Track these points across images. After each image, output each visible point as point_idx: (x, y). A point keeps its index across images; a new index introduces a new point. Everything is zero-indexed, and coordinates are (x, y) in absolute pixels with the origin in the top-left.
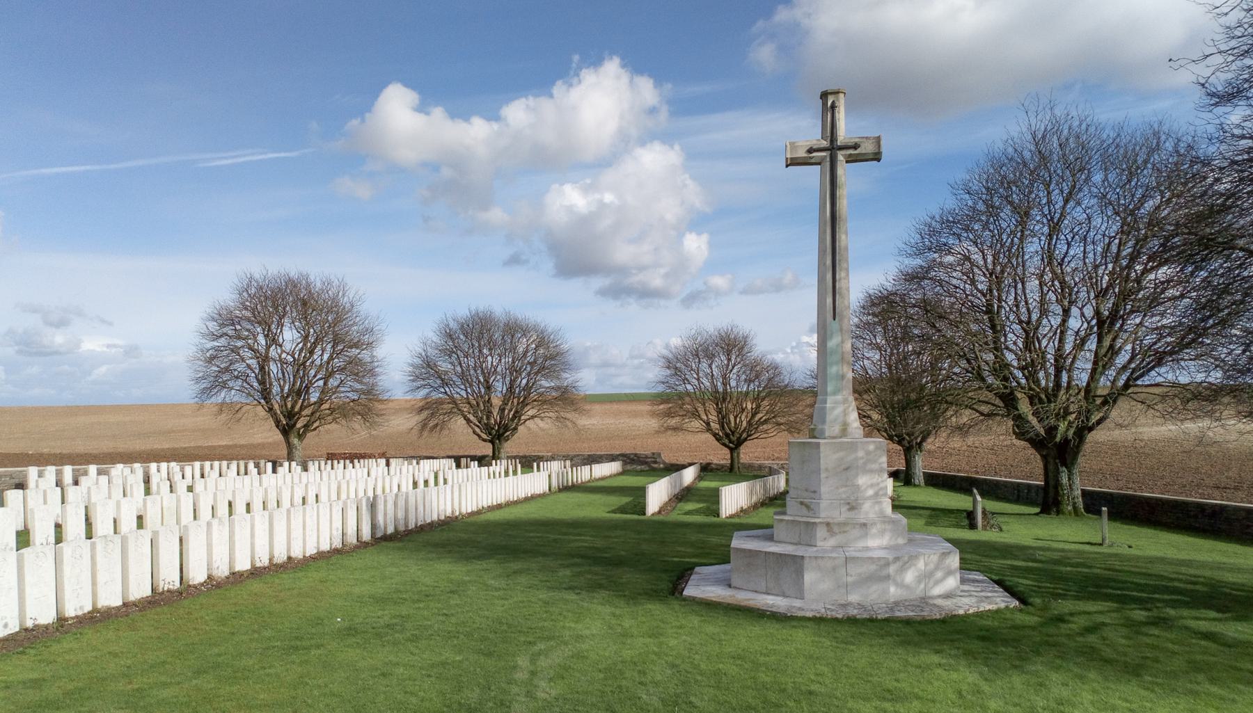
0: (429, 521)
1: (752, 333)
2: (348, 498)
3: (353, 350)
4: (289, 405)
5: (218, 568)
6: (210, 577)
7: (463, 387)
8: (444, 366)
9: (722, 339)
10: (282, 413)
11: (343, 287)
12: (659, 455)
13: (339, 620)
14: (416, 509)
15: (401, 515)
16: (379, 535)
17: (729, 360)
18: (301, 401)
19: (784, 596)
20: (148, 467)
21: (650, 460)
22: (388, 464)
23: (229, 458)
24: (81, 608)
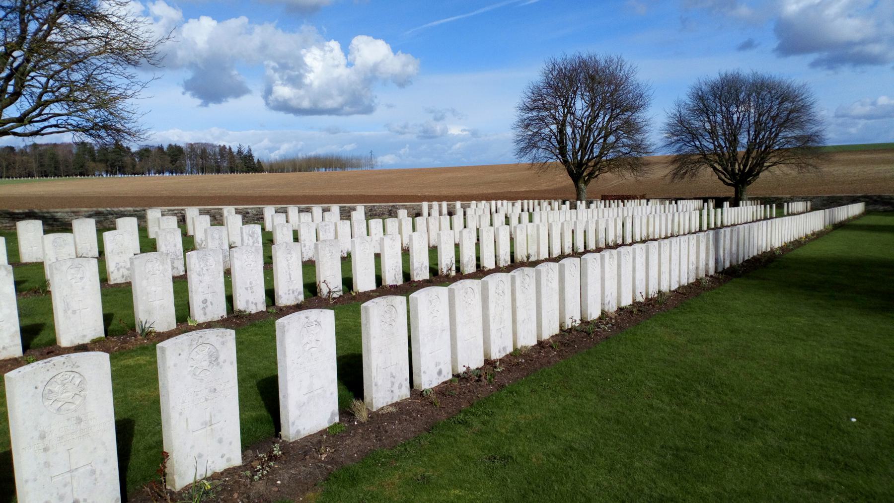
6: (603, 312)
11: (621, 62)
24: (504, 349)
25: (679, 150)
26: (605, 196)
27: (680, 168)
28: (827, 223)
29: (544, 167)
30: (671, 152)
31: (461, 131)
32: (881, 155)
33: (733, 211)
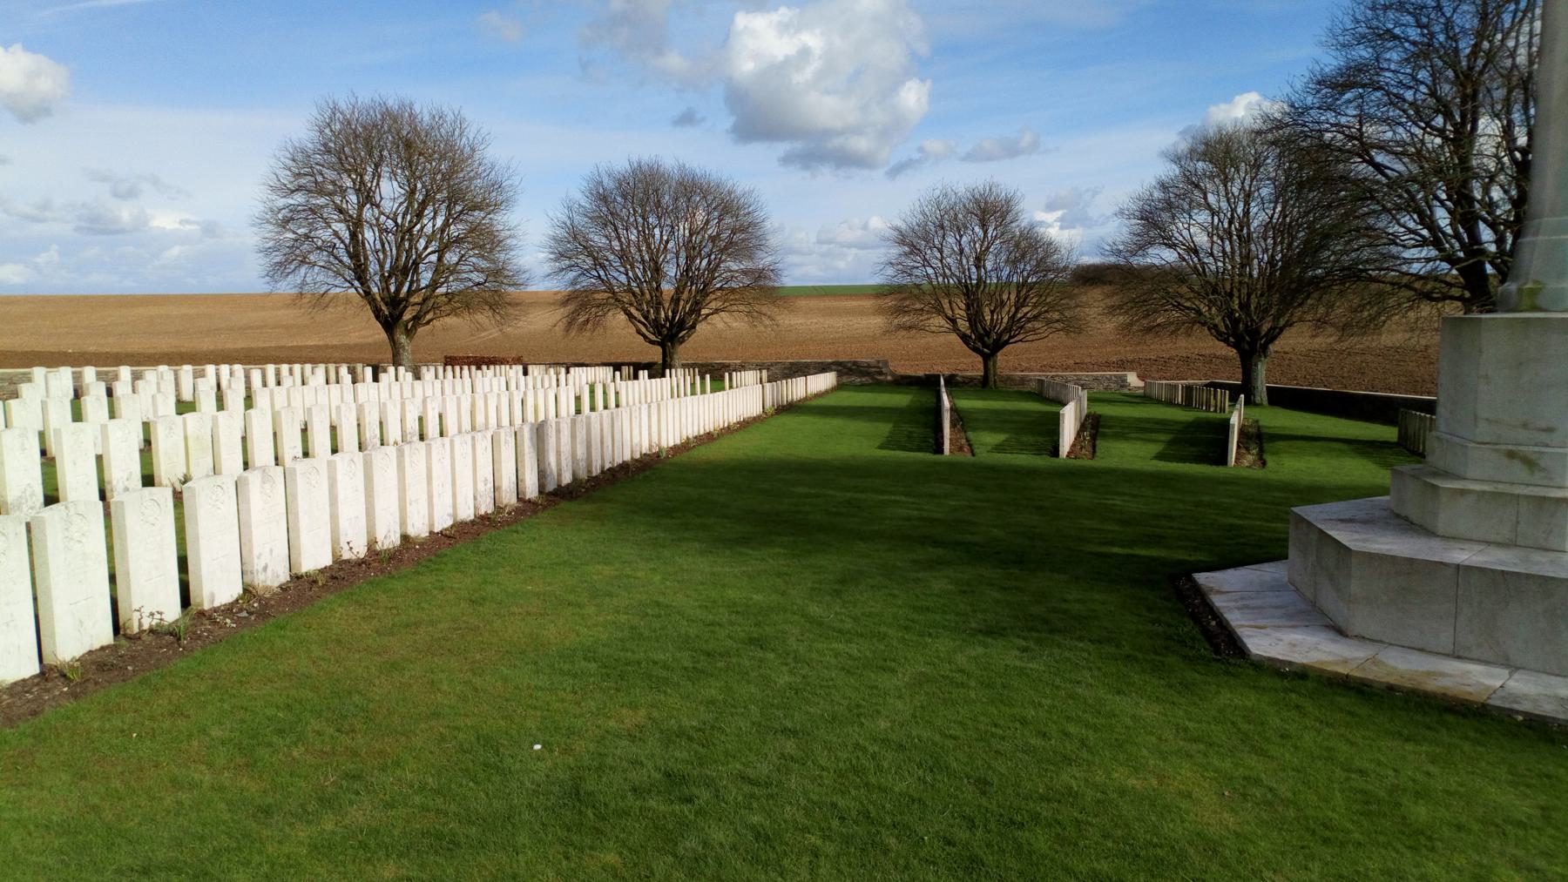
0: (619, 461)
1: (1019, 194)
2: (499, 426)
3: (476, 213)
4: (392, 288)
5: (265, 568)
7: (622, 269)
8: (598, 240)
9: (977, 202)
10: (382, 299)
11: (460, 121)
12: (886, 363)
13: (537, 747)
14: (602, 443)
15: (581, 452)
16: (551, 487)
17: (986, 233)
18: (407, 284)
19: (1507, 663)
20: (203, 370)
21: (873, 370)
22: (525, 373)
23: (314, 361)
25: (574, 282)
26: (450, 357)
27: (576, 312)
28: (768, 404)
29: (321, 301)
30: (558, 285)
31: (181, 222)
32: (860, 303)
33: (654, 384)
